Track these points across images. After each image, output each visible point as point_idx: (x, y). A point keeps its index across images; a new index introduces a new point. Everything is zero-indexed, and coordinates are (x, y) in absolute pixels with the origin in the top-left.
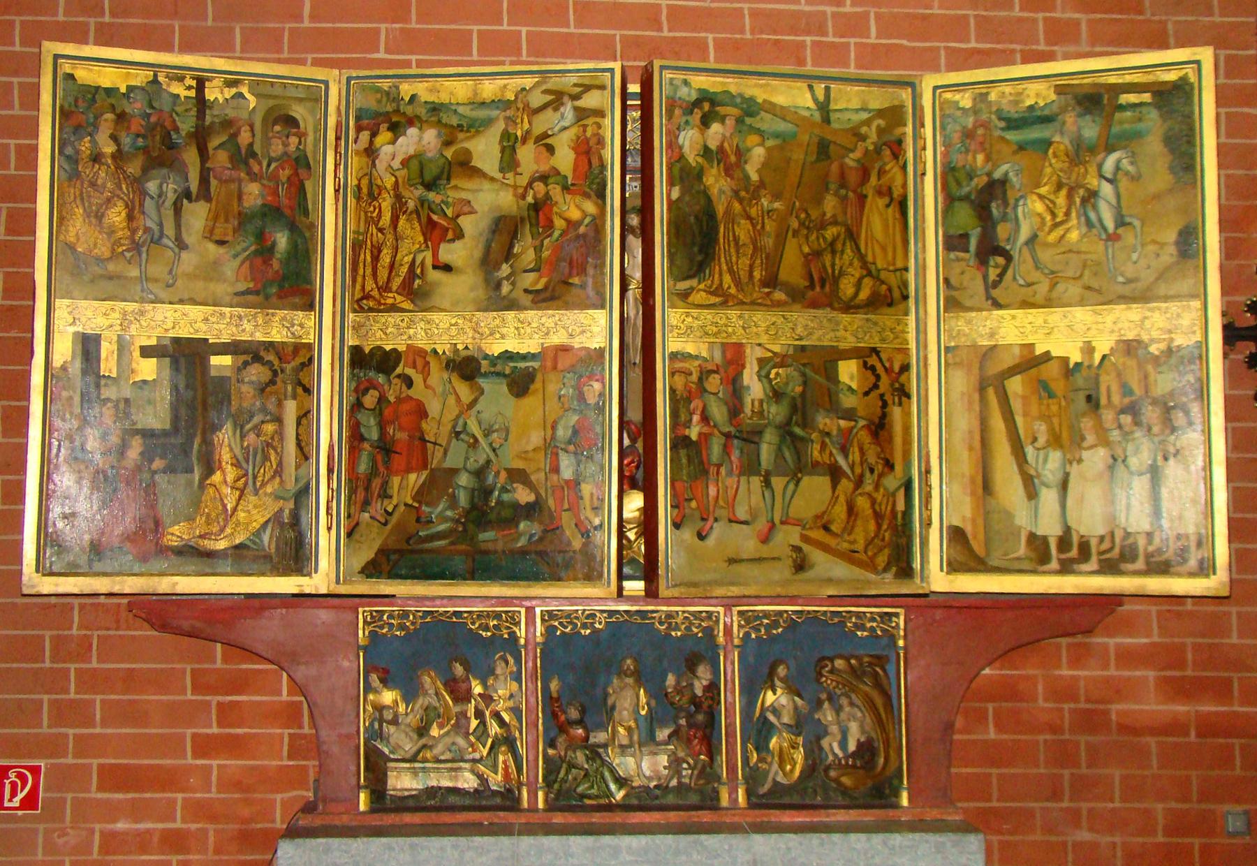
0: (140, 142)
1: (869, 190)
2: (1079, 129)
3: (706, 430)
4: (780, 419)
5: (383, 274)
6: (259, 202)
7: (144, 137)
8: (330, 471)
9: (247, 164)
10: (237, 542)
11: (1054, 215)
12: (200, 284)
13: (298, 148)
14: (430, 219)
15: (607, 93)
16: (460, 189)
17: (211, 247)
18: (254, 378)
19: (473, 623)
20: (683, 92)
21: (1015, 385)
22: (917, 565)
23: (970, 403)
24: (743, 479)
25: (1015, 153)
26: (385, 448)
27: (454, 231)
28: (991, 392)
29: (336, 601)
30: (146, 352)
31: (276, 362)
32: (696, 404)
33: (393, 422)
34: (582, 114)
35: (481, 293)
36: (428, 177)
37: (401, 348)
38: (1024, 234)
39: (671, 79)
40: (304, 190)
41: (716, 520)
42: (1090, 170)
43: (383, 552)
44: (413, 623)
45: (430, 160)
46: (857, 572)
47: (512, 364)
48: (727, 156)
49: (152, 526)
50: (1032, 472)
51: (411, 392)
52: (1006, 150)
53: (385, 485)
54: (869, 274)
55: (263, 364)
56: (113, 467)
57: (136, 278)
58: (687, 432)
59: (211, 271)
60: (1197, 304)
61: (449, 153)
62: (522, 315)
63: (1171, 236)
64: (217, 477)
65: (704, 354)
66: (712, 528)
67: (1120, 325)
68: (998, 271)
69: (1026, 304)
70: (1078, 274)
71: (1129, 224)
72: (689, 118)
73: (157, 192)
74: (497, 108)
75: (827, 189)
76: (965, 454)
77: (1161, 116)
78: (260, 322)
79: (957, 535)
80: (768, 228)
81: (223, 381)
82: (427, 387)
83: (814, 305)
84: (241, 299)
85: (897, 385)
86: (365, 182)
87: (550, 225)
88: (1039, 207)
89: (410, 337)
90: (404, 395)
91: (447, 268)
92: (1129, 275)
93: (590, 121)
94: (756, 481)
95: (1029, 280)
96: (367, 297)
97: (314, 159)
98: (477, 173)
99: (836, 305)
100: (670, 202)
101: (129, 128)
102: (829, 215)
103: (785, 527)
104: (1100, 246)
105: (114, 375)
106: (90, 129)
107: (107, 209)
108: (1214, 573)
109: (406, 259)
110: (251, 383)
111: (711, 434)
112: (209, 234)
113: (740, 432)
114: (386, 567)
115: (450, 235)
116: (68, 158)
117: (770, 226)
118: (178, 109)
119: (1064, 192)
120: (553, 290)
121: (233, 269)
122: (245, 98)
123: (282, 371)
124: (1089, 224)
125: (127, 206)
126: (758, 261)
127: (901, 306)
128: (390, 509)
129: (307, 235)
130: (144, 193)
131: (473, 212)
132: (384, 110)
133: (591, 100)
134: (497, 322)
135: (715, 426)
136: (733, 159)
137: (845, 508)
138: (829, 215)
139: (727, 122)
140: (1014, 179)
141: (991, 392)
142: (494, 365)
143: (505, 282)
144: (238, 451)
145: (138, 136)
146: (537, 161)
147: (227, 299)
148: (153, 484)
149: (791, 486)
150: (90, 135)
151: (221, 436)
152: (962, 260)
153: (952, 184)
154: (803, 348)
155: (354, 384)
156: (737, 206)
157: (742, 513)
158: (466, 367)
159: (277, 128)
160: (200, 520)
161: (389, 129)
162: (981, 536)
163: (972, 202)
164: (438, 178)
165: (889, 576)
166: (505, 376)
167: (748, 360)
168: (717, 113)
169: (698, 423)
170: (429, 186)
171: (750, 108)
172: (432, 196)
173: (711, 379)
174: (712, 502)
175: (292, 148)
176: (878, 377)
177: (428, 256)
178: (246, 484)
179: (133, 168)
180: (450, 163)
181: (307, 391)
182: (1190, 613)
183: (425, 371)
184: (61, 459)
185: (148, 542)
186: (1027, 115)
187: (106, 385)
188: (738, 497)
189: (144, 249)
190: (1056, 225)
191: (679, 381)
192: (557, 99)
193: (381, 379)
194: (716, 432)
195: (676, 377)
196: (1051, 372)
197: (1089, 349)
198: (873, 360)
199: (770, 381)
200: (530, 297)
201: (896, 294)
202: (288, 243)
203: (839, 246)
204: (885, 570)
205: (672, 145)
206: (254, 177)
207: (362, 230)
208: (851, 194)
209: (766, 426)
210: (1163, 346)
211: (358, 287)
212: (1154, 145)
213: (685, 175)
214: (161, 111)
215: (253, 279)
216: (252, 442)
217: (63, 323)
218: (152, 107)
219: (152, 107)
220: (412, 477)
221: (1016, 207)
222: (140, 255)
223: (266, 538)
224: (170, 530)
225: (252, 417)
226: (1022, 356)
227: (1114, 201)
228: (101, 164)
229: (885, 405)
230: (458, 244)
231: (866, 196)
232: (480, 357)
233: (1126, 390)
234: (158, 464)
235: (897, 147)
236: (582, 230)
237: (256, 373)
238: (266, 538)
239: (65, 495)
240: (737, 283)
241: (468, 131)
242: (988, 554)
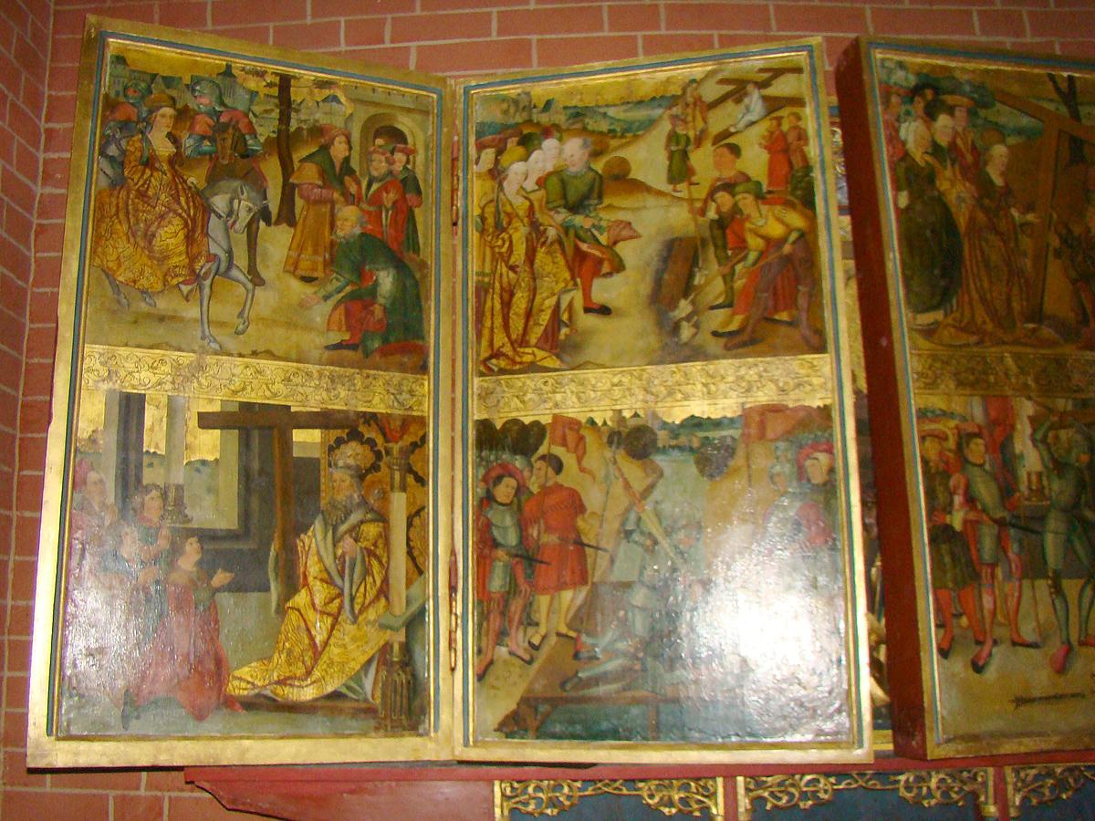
0: (206, 146)
3: (972, 516)
4: (1065, 498)
5: (517, 324)
6: (358, 231)
7: (213, 140)
8: (452, 589)
9: (342, 183)
10: (330, 689)
12: (280, 332)
13: (405, 168)
14: (577, 249)
15: (805, 77)
16: (616, 209)
17: (296, 285)
18: (351, 462)
19: (651, 796)
20: (899, 76)
26: (528, 557)
27: (611, 262)
29: (465, 770)
30: (206, 421)
31: (380, 441)
32: (956, 480)
33: (536, 521)
34: (773, 105)
35: (653, 341)
36: (573, 196)
37: (546, 420)
39: (883, 60)
40: (413, 217)
41: (995, 643)
43: (528, 701)
44: (569, 797)
45: (575, 177)
47: (702, 434)
48: (963, 156)
49: (212, 667)
51: (561, 479)
53: (528, 606)
55: (362, 443)
56: (157, 582)
57: (196, 320)
58: (948, 519)
59: (292, 317)
61: (599, 166)
62: (711, 367)
64: (301, 599)
66: (990, 655)
72: (909, 107)
73: (226, 210)
74: (660, 106)
78: (359, 385)
81: (312, 464)
82: (582, 470)
84: (336, 353)
86: (490, 210)
87: (742, 246)
89: (556, 405)
90: (550, 483)
91: (604, 311)
94: (1043, 586)
96: (497, 355)
97: (425, 180)
98: (639, 187)
101: (192, 128)
103: (1084, 649)
105: (162, 452)
106: (140, 126)
107: (159, 227)
109: (547, 303)
110: (348, 467)
112: (292, 267)
113: (1018, 517)
114: (532, 723)
115: (606, 268)
116: (111, 159)
118: (256, 109)
120: (753, 332)
121: (322, 317)
122: (339, 102)
123: (388, 452)
125: (186, 225)
126: (1016, 290)
128: (536, 641)
129: (418, 276)
130: (208, 210)
131: (635, 236)
132: (512, 121)
133: (783, 87)
134: (678, 377)
135: (984, 510)
136: (969, 158)
139: (957, 113)
142: (676, 436)
143: (684, 324)
144: (329, 561)
145: (203, 138)
146: (718, 165)
147: (316, 354)
148: (213, 608)
150: (142, 133)
151: (307, 541)
155: (482, 471)
157: (1028, 631)
158: (636, 440)
159: (379, 141)
160: (279, 658)
161: (519, 144)
164: (586, 197)
166: (691, 450)
168: (943, 102)
169: (962, 505)
170: (575, 208)
172: (579, 220)
173: (972, 446)
174: (988, 620)
175: (398, 167)
177: (577, 297)
178: (341, 607)
179: (195, 178)
180: (601, 177)
181: (421, 481)
183: (579, 448)
184: (86, 568)
185: (209, 689)
187: (151, 465)
188: (1022, 611)
189: (208, 283)
191: (932, 448)
192: (738, 89)
193: (519, 462)
194: (985, 517)
195: (928, 443)
200: (722, 341)
202: (393, 284)
205: (894, 138)
206: (351, 199)
207: (487, 270)
209: (1048, 509)
211: (485, 343)
213: (915, 178)
214: (234, 109)
215: (349, 328)
216: (347, 548)
217: (91, 381)
218: (222, 104)
219: (222, 104)
220: (567, 595)
222: (201, 290)
223: (368, 684)
224: (237, 673)
225: (347, 514)
228: (153, 169)
230: (617, 278)
232: (656, 427)
234: (221, 578)
236: (787, 249)
237: (352, 454)
238: (368, 684)
239: (89, 623)
240: (994, 315)
241: (623, 136)
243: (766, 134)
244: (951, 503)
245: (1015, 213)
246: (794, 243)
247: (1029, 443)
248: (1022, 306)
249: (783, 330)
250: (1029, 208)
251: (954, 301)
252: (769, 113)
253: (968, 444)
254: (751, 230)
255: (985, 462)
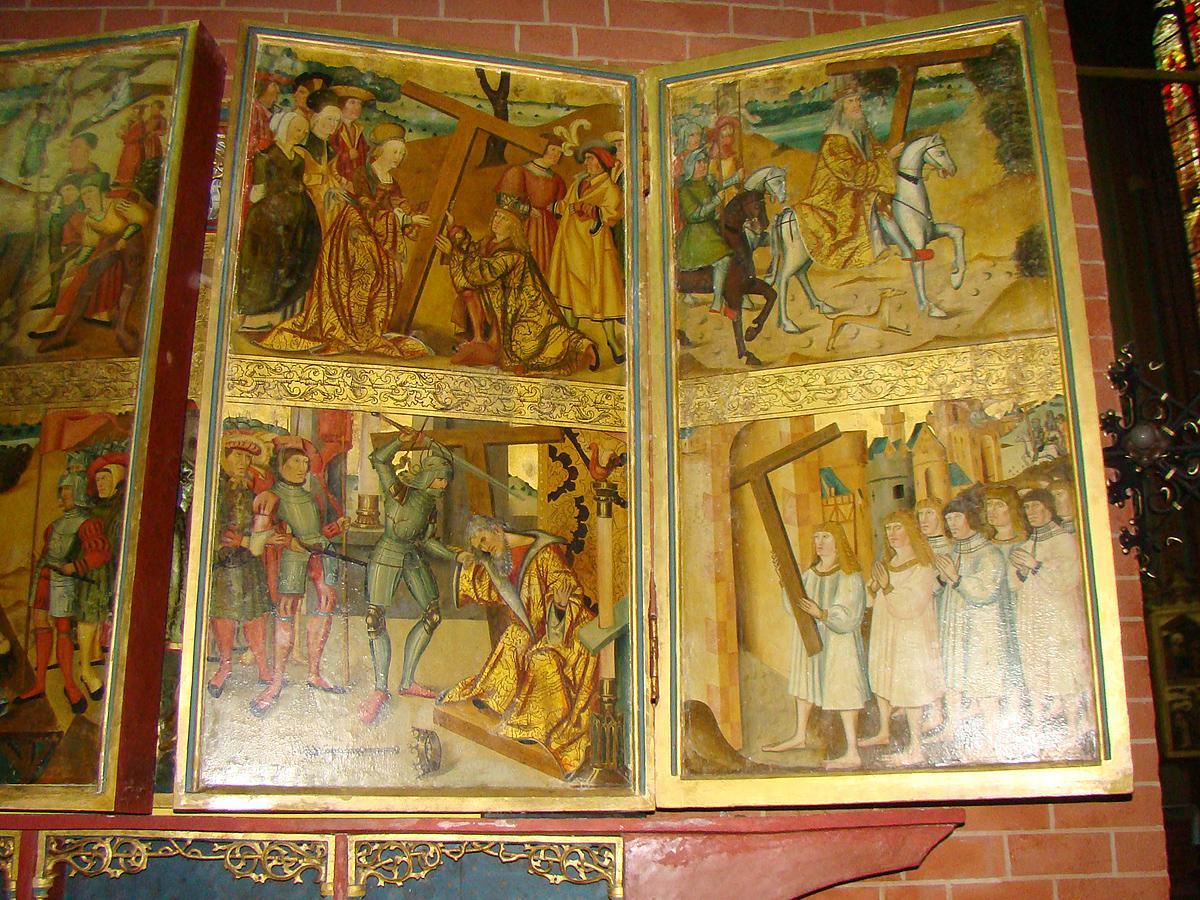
1: (564, 207)
2: (865, 115)
3: (277, 540)
11: (834, 231)
21: (785, 479)
22: (633, 765)
23: (717, 512)
24: (338, 620)
25: (774, 155)
28: (748, 489)
34: (139, 93)
38: (793, 259)
42: (883, 168)
46: (533, 777)
50: (814, 611)
52: (763, 152)
54: (563, 322)
60: (1054, 341)
63: (1008, 248)
65: (283, 424)
67: (940, 379)
68: (756, 315)
69: (797, 359)
70: (873, 311)
71: (946, 235)
72: (289, 97)
75: (499, 202)
76: (710, 589)
77: (980, 89)
79: (698, 716)
80: (401, 248)
83: (471, 361)
85: (604, 486)
88: (814, 223)
92: (947, 306)
93: (149, 101)
94: (360, 623)
95: (801, 324)
99: (508, 363)
100: (248, 207)
102: (500, 238)
104: (905, 269)
108: (1108, 757)
111: (287, 547)
117: (406, 246)
119: (847, 199)
124: (886, 238)
126: (383, 294)
127: (613, 372)
136: (353, 153)
137: (513, 672)
138: (500, 238)
139: (348, 105)
140: (776, 189)
141: (748, 489)
149: (421, 634)
152: (705, 303)
153: (687, 201)
154: (450, 423)
156: (354, 217)
162: (736, 717)
163: (716, 224)
165: (587, 782)
167: (356, 437)
169: (266, 528)
171: (383, 90)
173: (291, 462)
176: (573, 472)
182: (1054, 838)
186: (790, 104)
190: (838, 245)
194: (294, 542)
195: (232, 457)
196: (839, 454)
197: (895, 418)
198: (565, 447)
199: (393, 469)
200: (38, 343)
201: (605, 353)
203: (515, 281)
204: (580, 772)
205: (261, 128)
208: (535, 212)
209: (381, 538)
210: (1007, 405)
212: (973, 126)
213: (271, 166)
221: (779, 224)
226: (793, 435)
227: (920, 207)
229: (584, 514)
231: (559, 216)
233: (953, 475)
235: (608, 158)
236: (121, 244)
240: (348, 323)
242: (746, 744)
243: (126, 123)
244: (253, 524)
245: (399, 213)
246: (127, 239)
247: (368, 463)
248: (387, 313)
249: (100, 330)
250: (420, 208)
251: (298, 304)
252: (135, 101)
253: (285, 461)
254: (90, 226)
255: (305, 481)
